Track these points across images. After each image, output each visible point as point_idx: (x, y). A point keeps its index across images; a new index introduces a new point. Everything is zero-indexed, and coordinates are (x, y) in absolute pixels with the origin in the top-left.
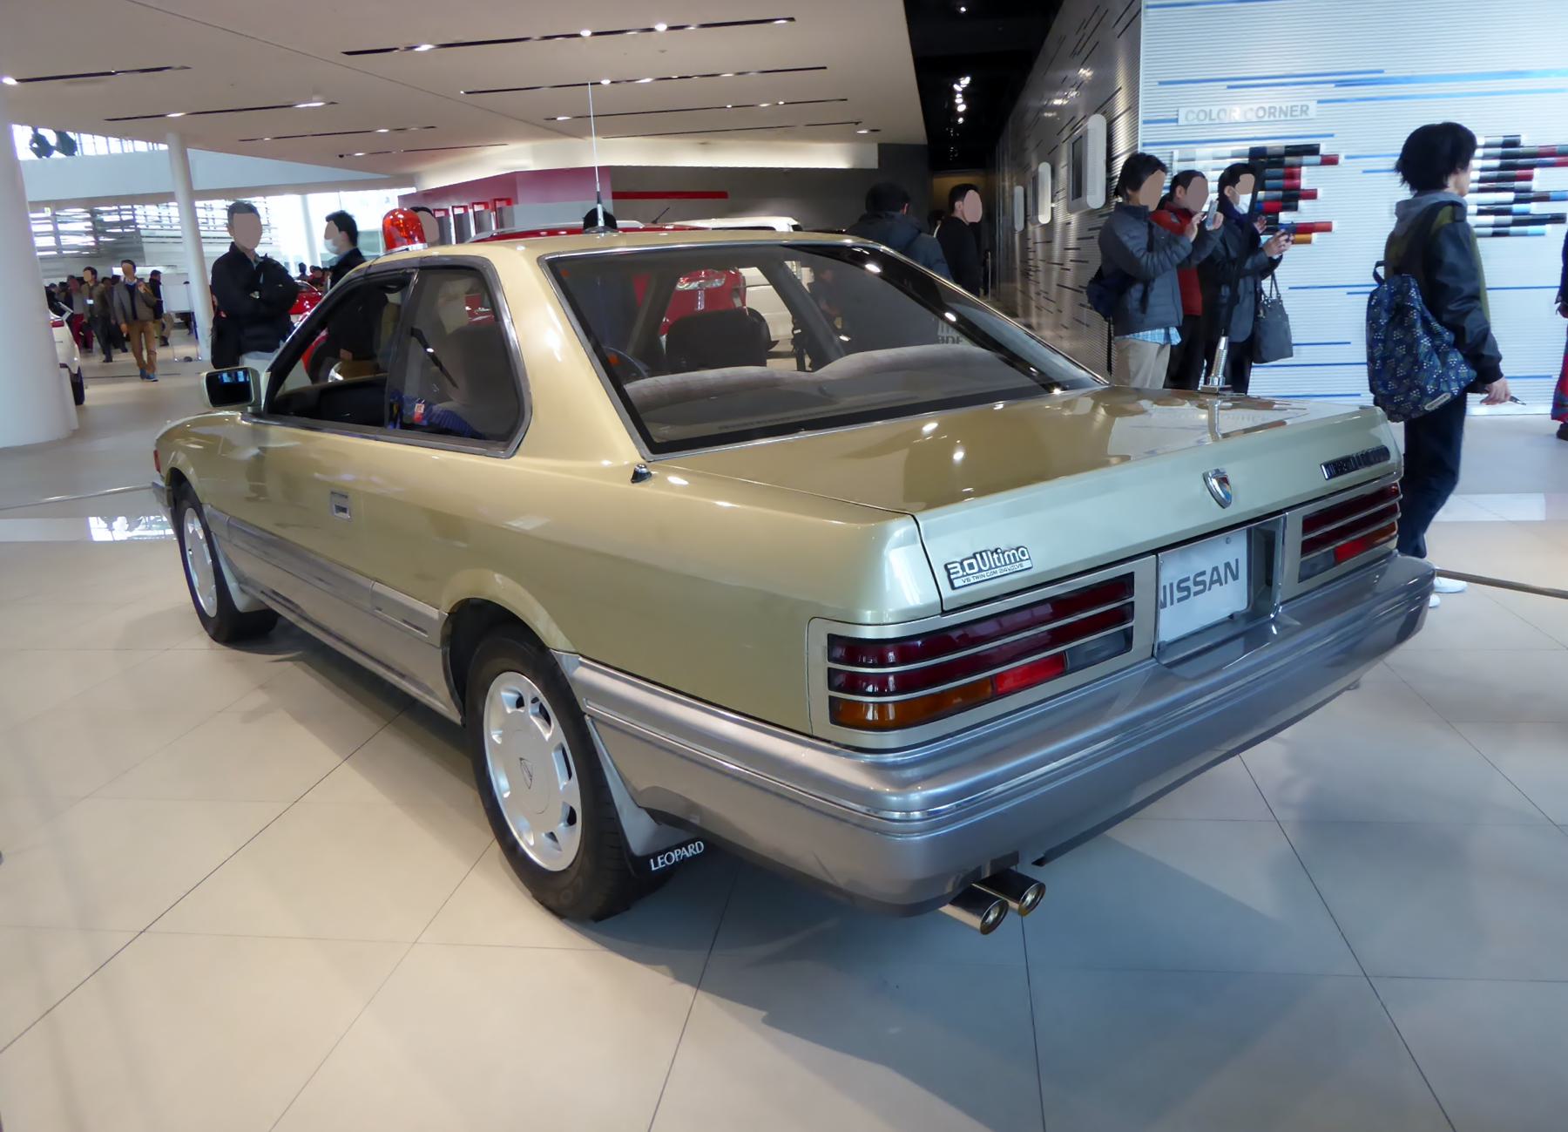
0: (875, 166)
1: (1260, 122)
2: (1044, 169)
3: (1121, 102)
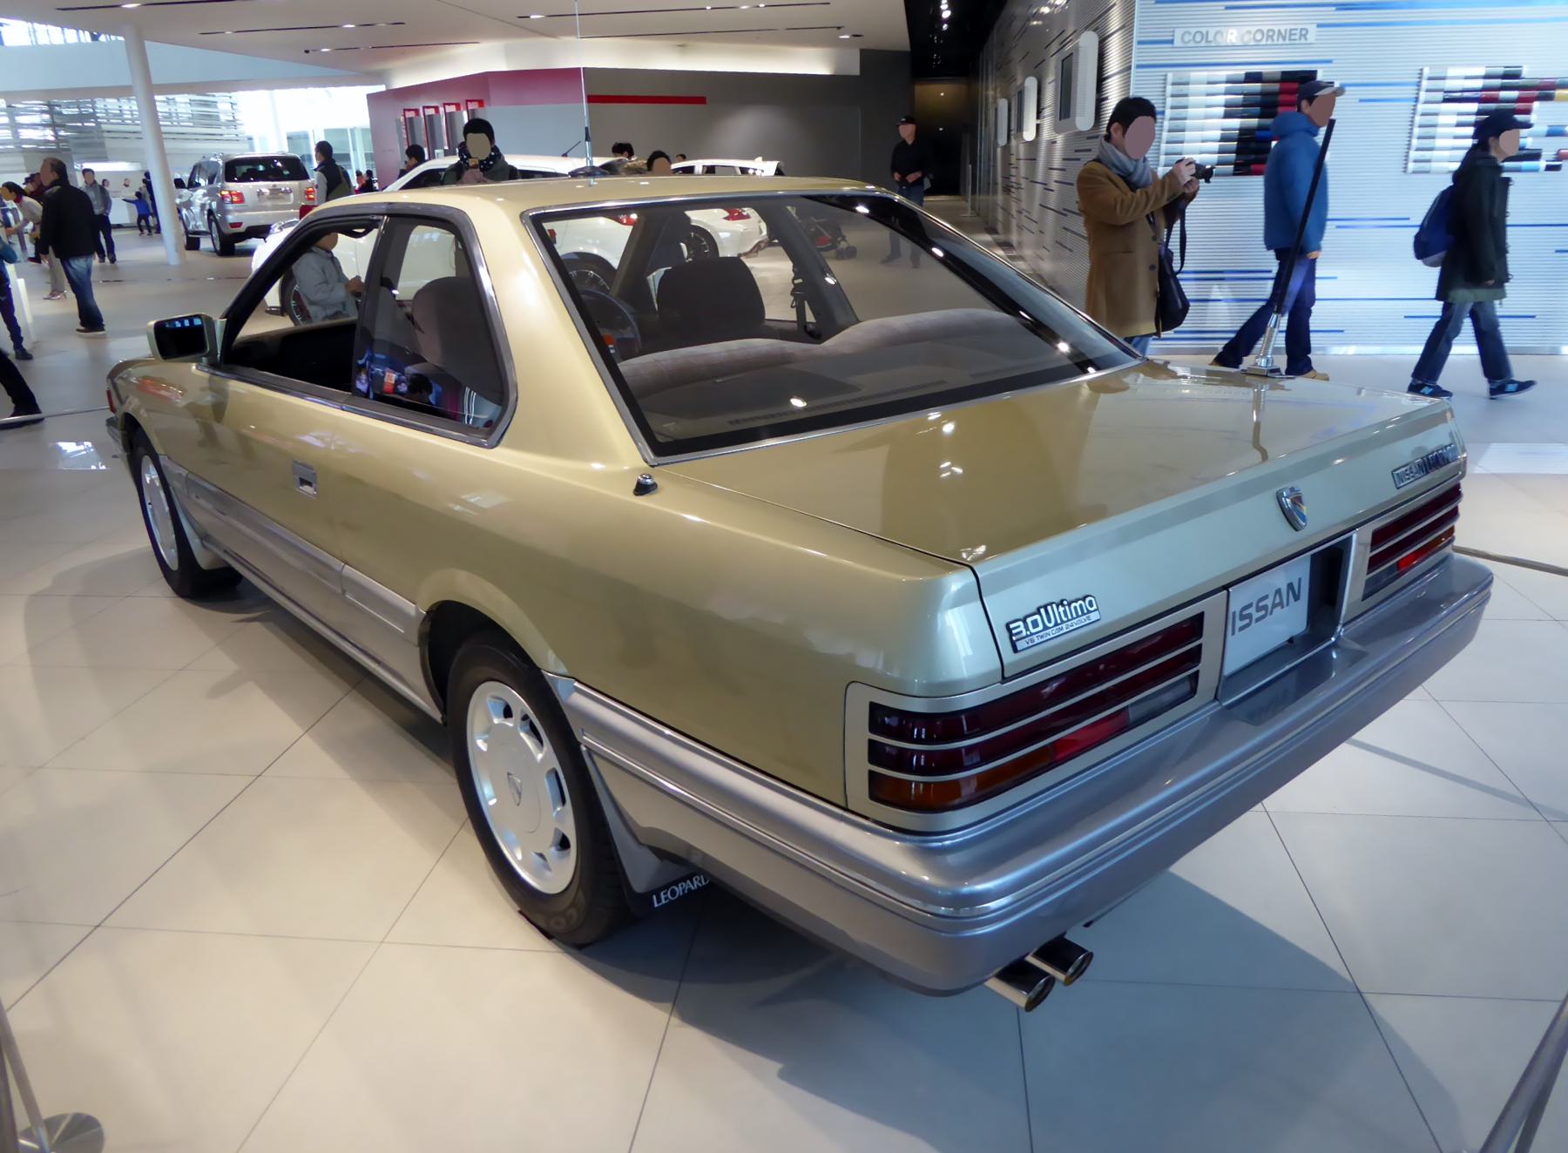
0: (856, 72)
1: (1257, 46)
2: (1031, 84)
3: (1115, 20)
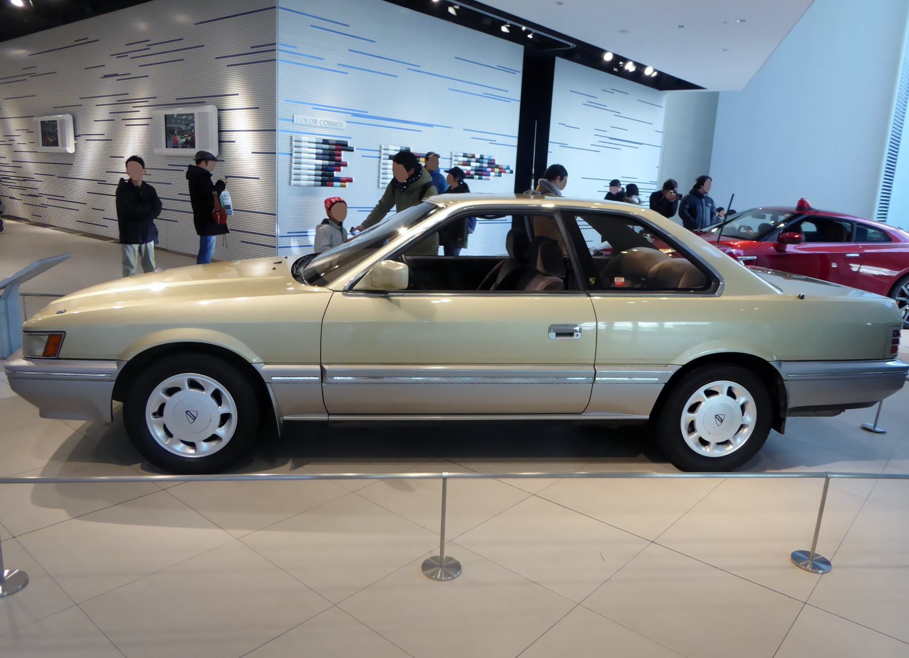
1: (326, 128)
